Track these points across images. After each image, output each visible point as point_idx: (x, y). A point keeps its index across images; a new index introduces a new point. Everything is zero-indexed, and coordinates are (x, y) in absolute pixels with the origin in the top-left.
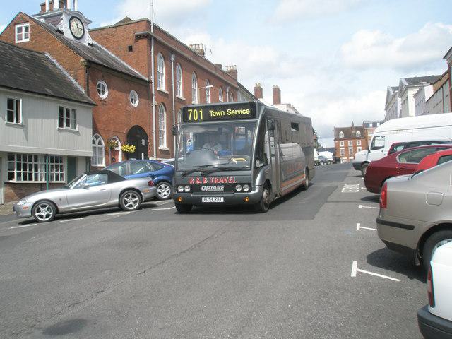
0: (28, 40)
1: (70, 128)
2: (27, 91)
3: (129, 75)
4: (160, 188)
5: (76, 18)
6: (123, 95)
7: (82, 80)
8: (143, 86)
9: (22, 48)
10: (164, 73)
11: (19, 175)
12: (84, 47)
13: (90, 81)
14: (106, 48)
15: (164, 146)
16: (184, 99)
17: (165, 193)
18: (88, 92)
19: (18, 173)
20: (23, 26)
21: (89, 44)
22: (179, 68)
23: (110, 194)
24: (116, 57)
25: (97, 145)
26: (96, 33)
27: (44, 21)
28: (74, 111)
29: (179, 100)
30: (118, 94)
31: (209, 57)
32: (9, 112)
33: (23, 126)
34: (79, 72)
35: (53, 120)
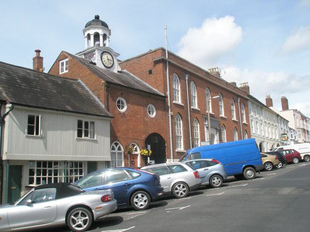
0: (67, 71)
1: (88, 138)
2: (45, 108)
3: (153, 94)
4: (137, 197)
5: (107, 52)
6: (141, 108)
7: (103, 98)
8: (160, 101)
9: (64, 78)
10: (179, 89)
11: (38, 180)
12: (113, 74)
13: (110, 99)
14: (133, 74)
15: (181, 148)
16: (199, 109)
17: (142, 203)
18: (108, 107)
19: (37, 178)
20: (64, 61)
21: (118, 72)
22: (192, 83)
23: (56, 212)
24: (141, 80)
25: (116, 150)
26: (121, 63)
27: (83, 57)
28: (93, 123)
29: (194, 111)
30: (136, 108)
31: (223, 77)
32: (29, 127)
33: (41, 138)
34: (101, 91)
35: (71, 132)
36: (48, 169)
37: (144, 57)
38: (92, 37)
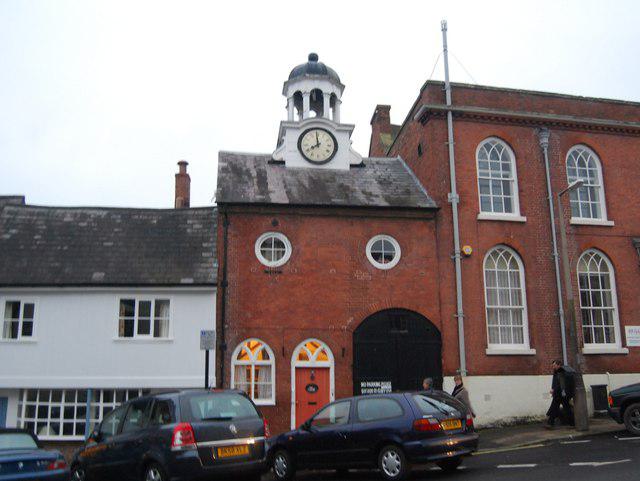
36: (51, 404)
37: (57, 281)
38: (306, 101)
